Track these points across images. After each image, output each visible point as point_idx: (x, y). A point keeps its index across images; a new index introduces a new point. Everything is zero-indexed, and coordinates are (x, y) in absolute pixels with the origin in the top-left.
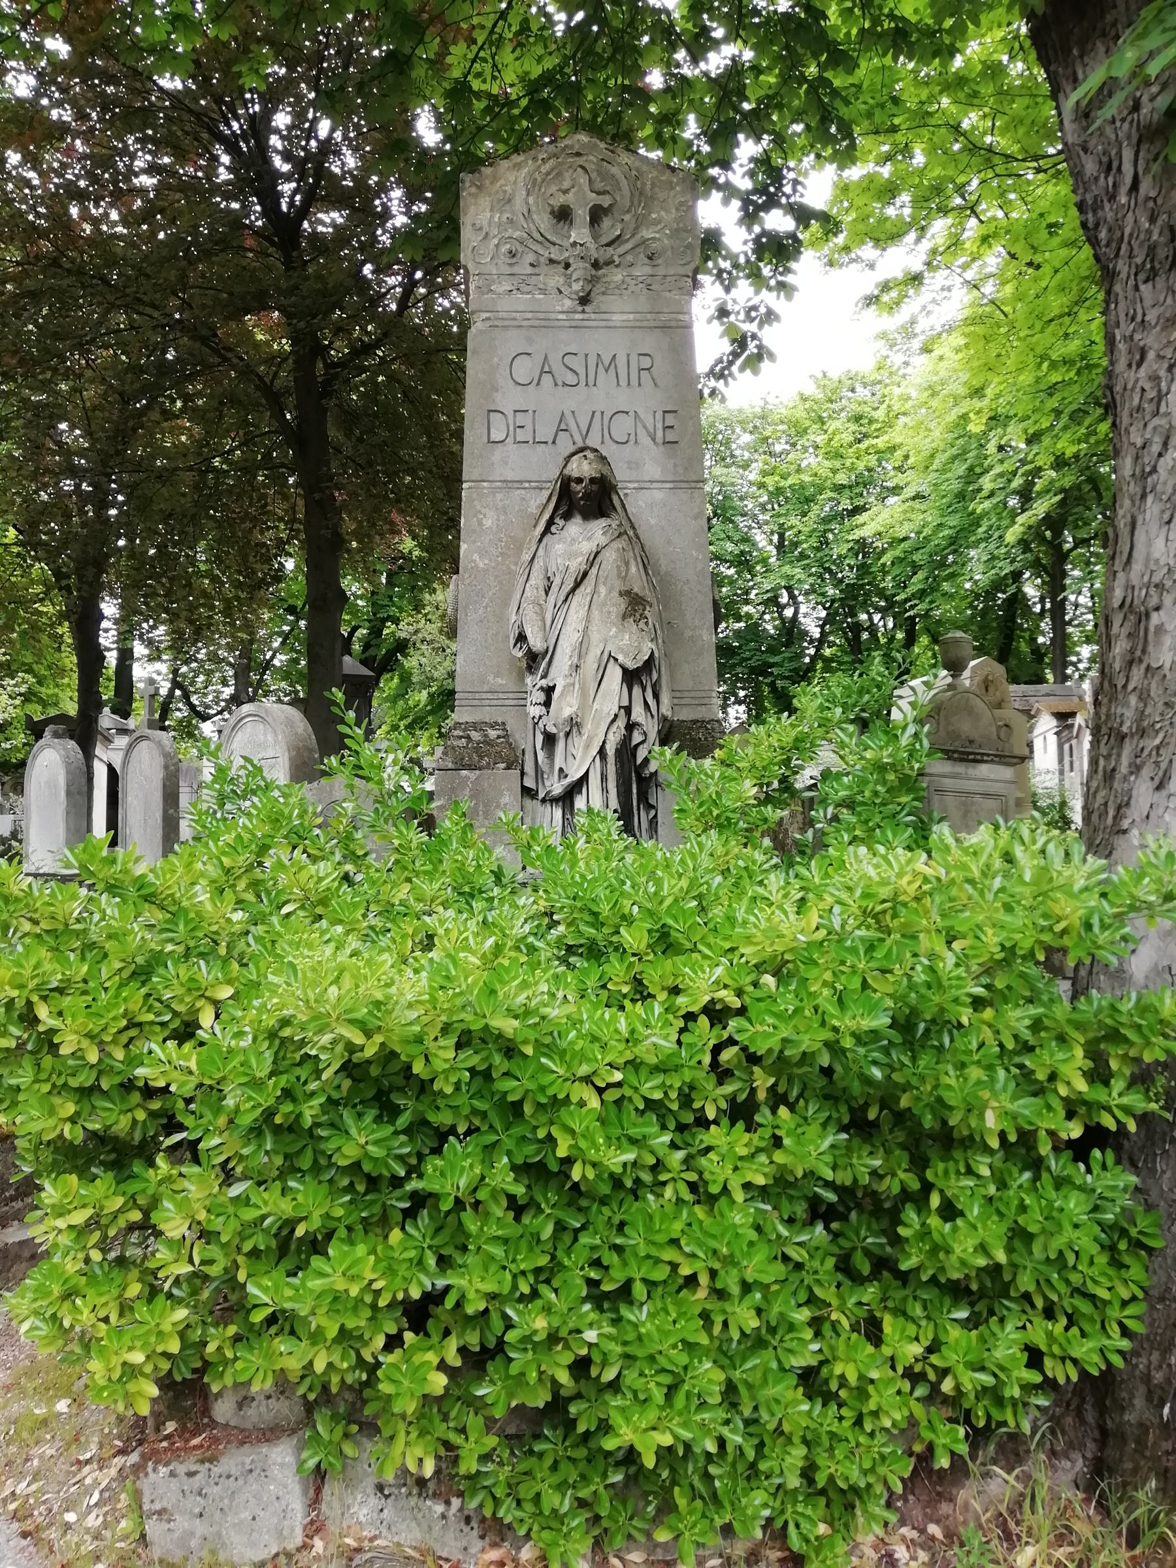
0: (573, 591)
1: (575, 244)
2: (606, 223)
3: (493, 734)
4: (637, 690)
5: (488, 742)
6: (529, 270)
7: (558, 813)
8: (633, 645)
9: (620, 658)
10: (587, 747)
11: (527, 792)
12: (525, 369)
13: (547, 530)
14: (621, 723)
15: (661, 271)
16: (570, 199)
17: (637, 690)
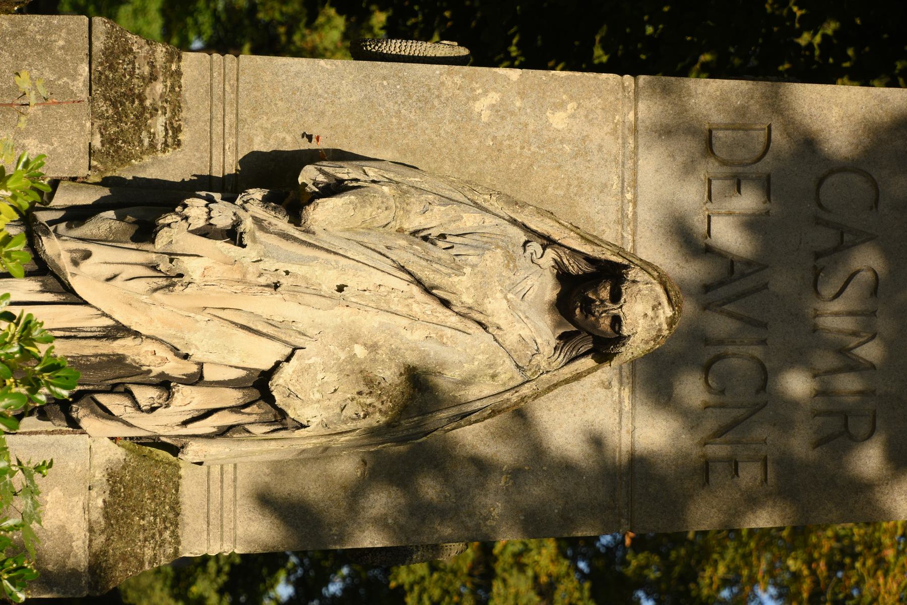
3: (159, 124)
4: (233, 397)
5: (142, 117)
9: (288, 369)
14: (174, 367)
17: (233, 397)
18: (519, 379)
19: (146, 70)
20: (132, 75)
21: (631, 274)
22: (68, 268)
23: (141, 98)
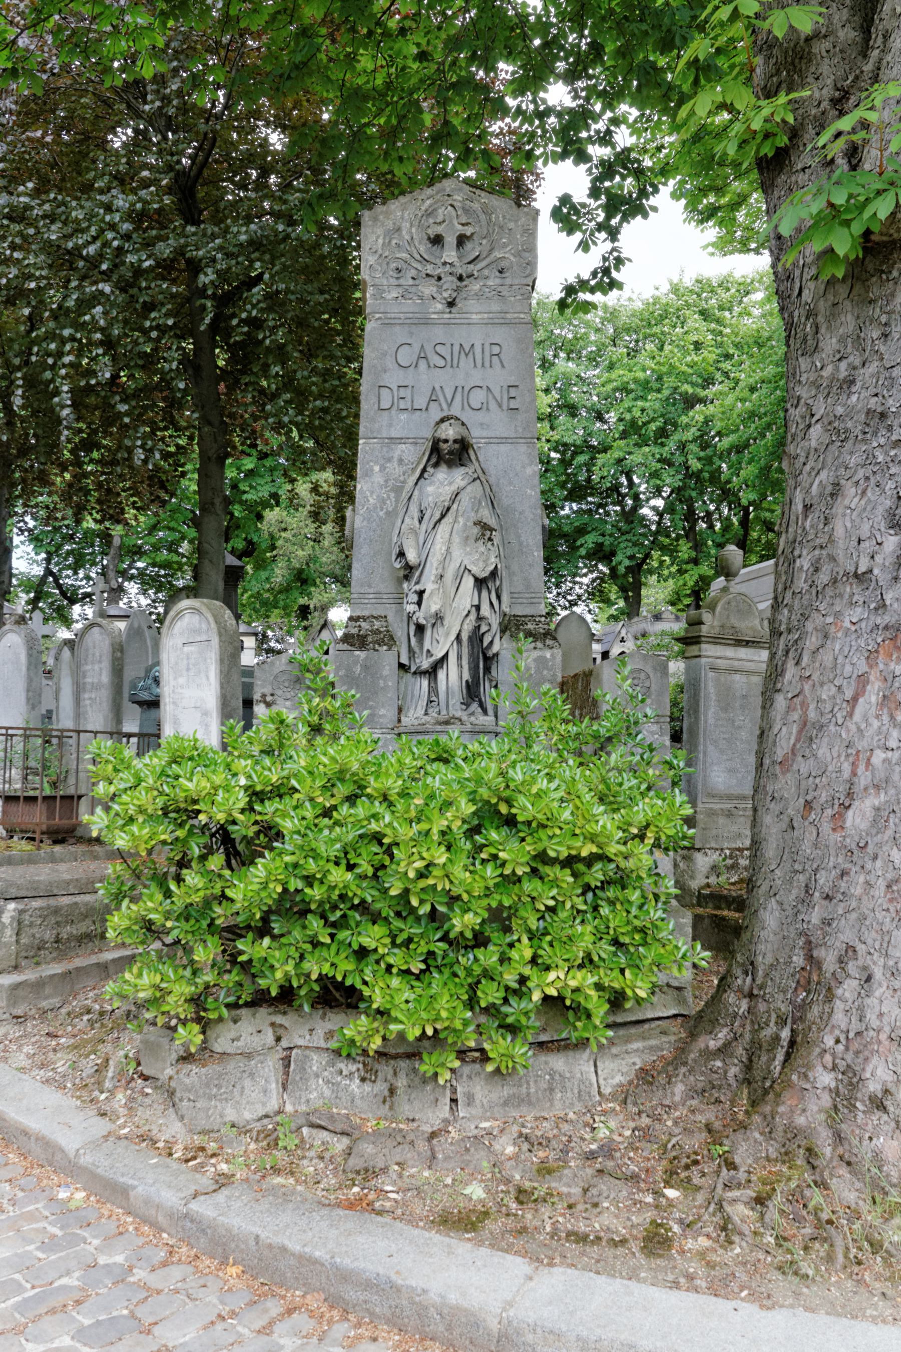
0: (440, 520)
2: (469, 246)
4: (485, 593)
6: (411, 282)
7: (425, 683)
14: (473, 616)
15: (508, 281)
17: (485, 593)
22: (434, 658)
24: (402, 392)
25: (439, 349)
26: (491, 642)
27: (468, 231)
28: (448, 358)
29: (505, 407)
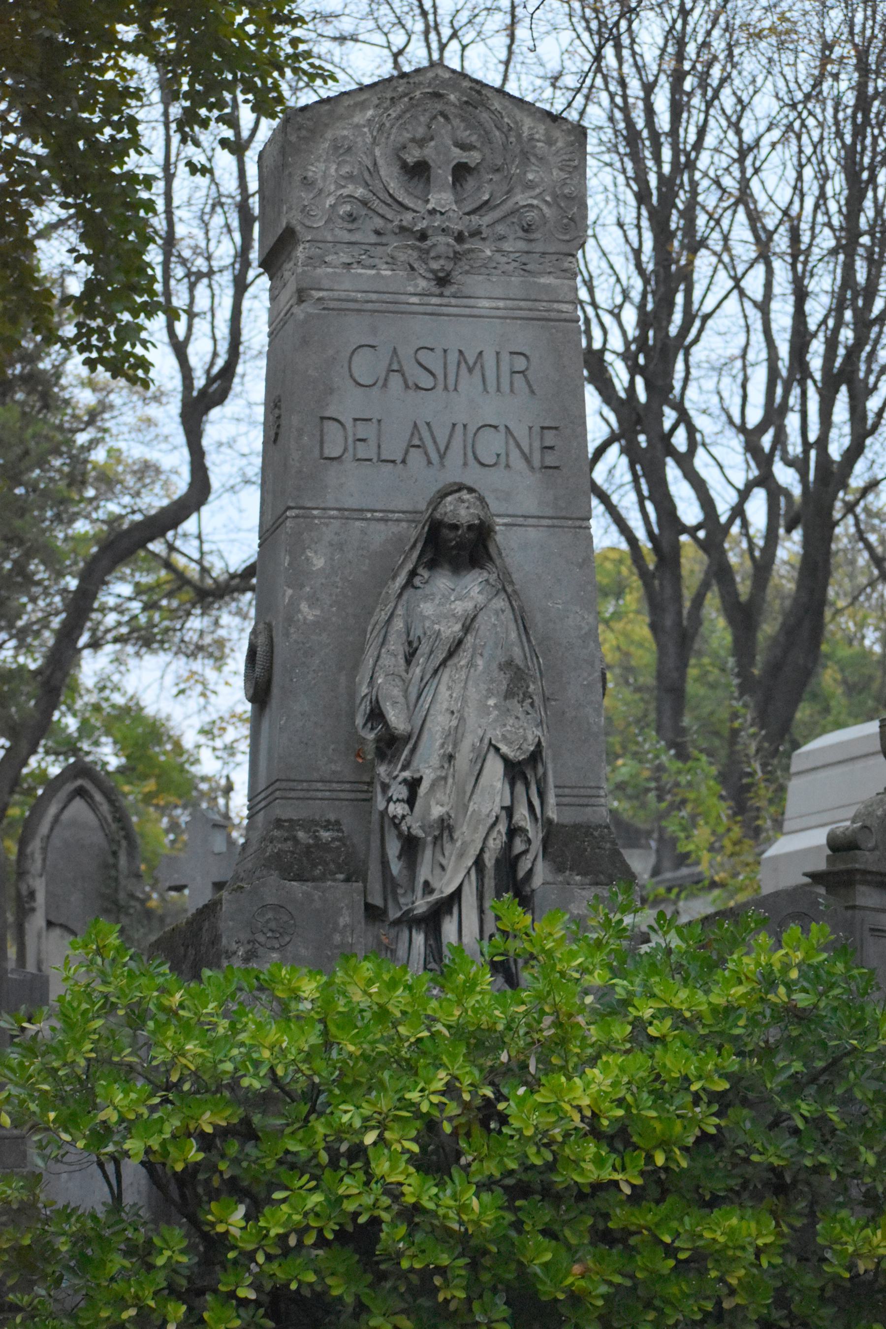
0: (444, 663)
1: (433, 212)
2: (471, 183)
3: (325, 835)
4: (520, 787)
5: (320, 846)
6: (373, 239)
7: (419, 939)
8: (520, 734)
9: (504, 749)
10: (461, 855)
11: (373, 914)
12: (365, 367)
13: (409, 583)
14: (502, 827)
15: (539, 247)
16: (429, 152)
17: (520, 787)
18: (503, 596)
19: (290, 843)
20: (293, 852)
21: (438, 516)
22: (435, 896)
23: (308, 846)
24: (362, 430)
25: (423, 356)
26: (531, 871)
27: (473, 158)
28: (441, 377)
29: (537, 463)
